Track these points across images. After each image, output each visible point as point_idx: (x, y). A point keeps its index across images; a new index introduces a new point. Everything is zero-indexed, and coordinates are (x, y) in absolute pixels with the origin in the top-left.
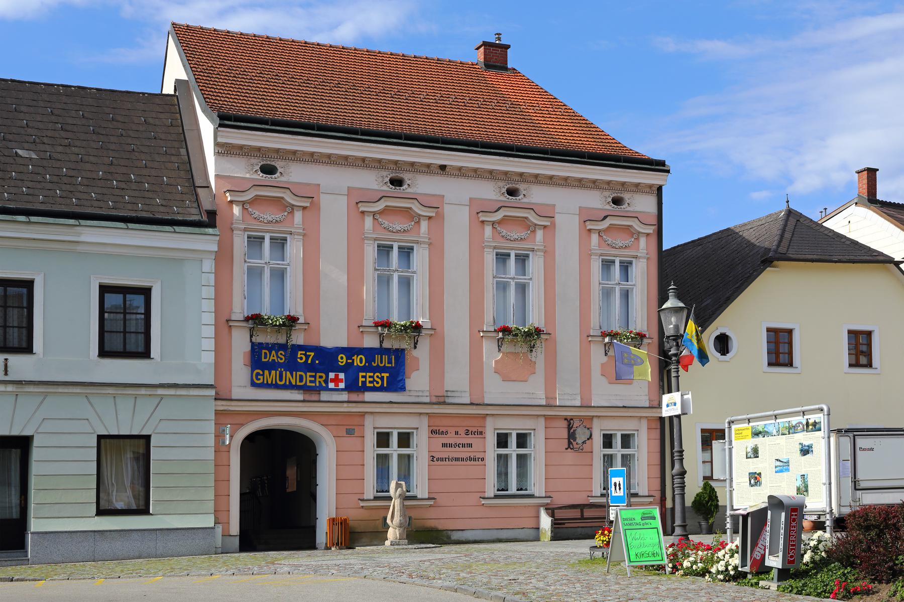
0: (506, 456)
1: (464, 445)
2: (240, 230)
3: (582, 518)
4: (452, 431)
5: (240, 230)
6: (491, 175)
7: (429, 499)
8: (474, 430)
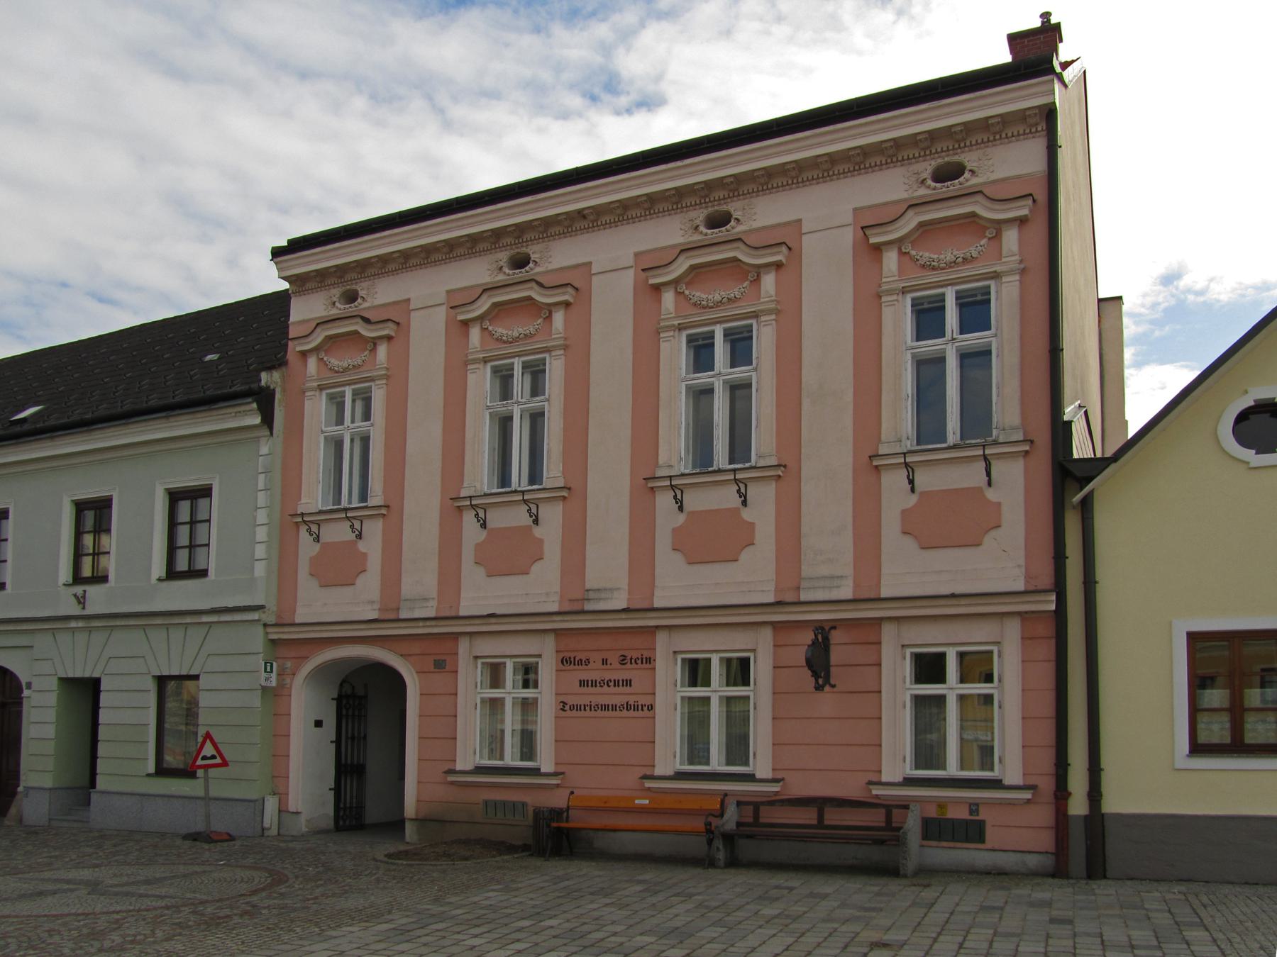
0: (941, 700)
1: (616, 683)
2: (311, 389)
3: (821, 824)
4: (596, 658)
5: (311, 389)
7: (555, 774)
8: (635, 655)
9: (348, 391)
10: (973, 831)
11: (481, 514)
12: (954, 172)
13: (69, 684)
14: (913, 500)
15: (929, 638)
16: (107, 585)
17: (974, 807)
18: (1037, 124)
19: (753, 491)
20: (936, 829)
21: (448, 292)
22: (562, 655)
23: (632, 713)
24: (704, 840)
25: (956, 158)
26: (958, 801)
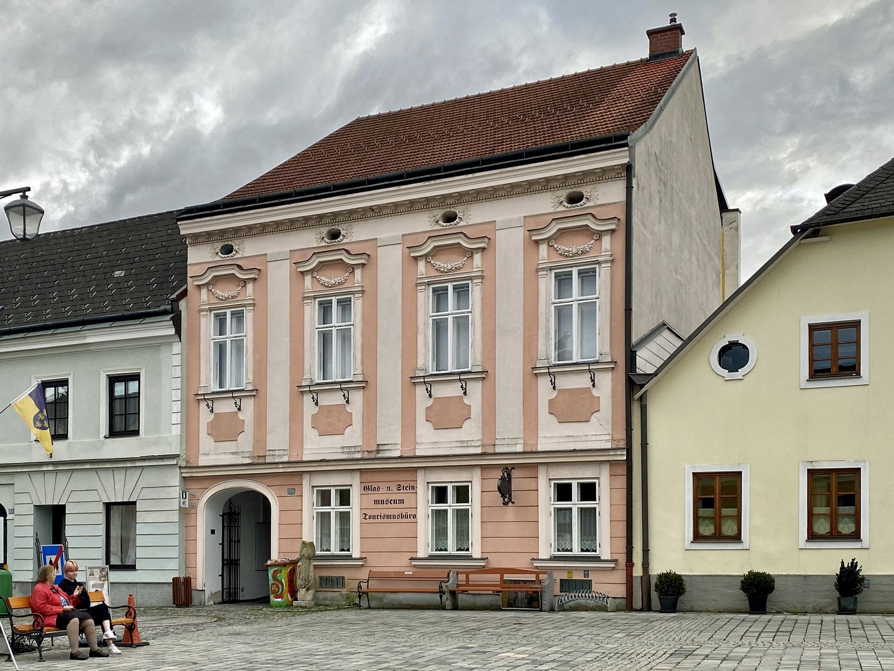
6: (545, 185)
9: (228, 312)
10: (586, 585)
11: (210, 404)
12: (575, 199)
13: (40, 509)
14: (554, 394)
15: (564, 475)
16: (68, 441)
17: (586, 572)
18: (621, 173)
19: (599, 377)
20: (567, 585)
21: (403, 235)
22: (364, 485)
23: (404, 520)
24: (438, 595)
25: (579, 190)
26: (577, 569)
